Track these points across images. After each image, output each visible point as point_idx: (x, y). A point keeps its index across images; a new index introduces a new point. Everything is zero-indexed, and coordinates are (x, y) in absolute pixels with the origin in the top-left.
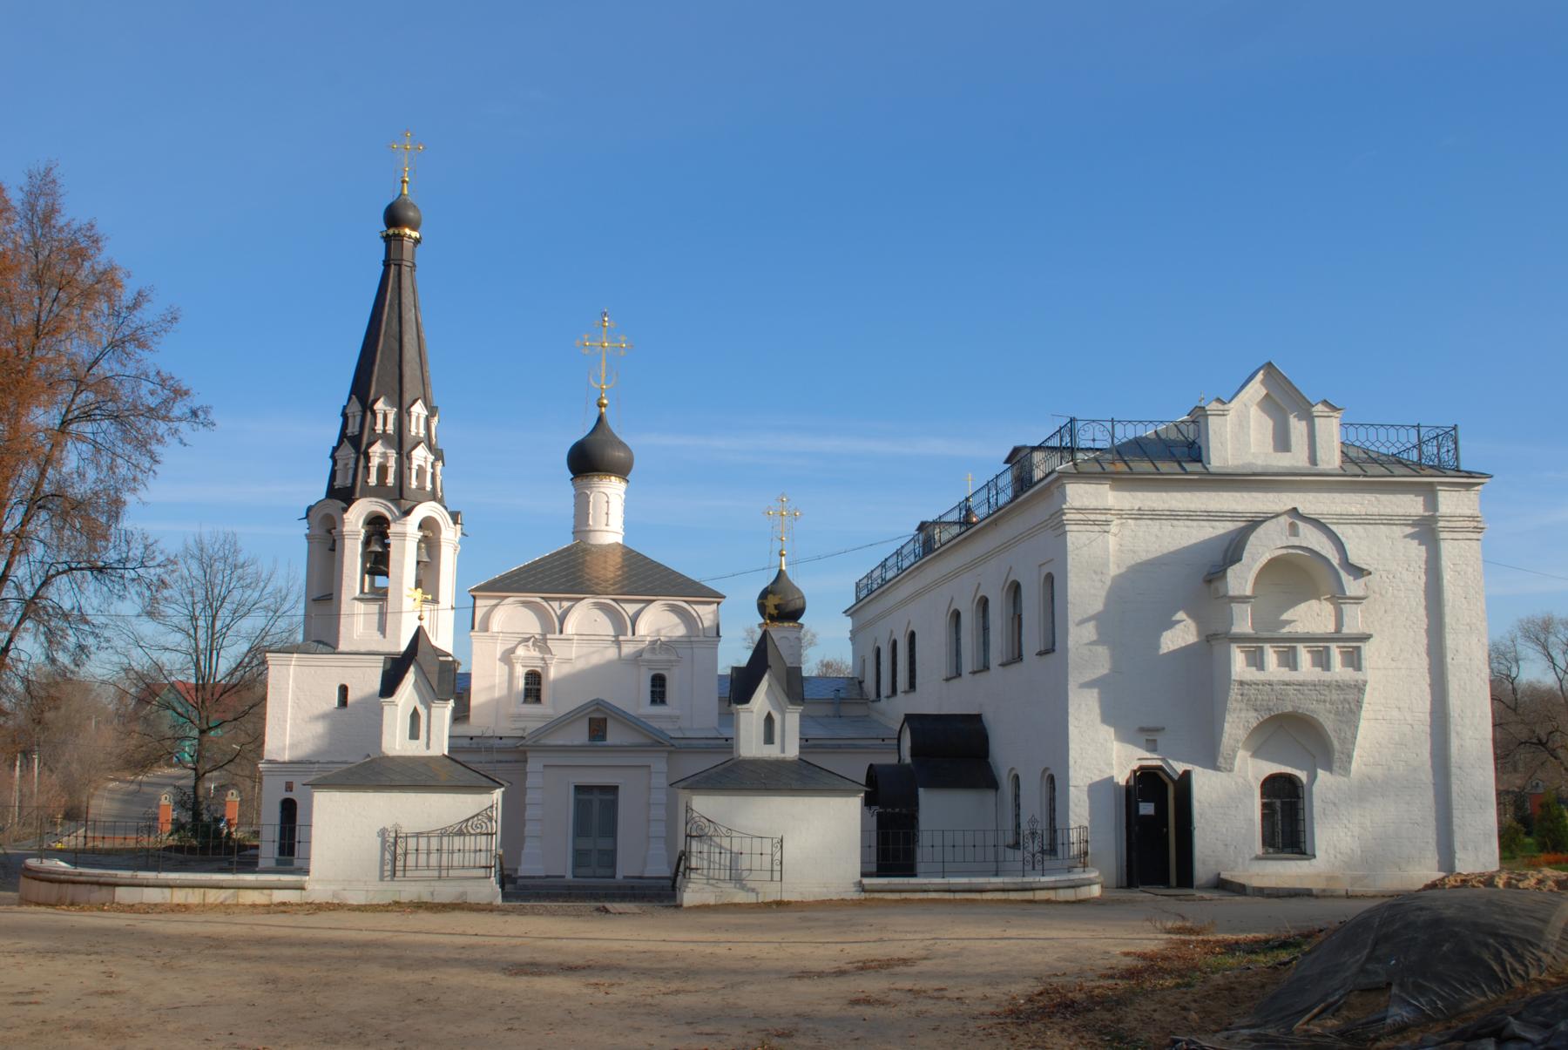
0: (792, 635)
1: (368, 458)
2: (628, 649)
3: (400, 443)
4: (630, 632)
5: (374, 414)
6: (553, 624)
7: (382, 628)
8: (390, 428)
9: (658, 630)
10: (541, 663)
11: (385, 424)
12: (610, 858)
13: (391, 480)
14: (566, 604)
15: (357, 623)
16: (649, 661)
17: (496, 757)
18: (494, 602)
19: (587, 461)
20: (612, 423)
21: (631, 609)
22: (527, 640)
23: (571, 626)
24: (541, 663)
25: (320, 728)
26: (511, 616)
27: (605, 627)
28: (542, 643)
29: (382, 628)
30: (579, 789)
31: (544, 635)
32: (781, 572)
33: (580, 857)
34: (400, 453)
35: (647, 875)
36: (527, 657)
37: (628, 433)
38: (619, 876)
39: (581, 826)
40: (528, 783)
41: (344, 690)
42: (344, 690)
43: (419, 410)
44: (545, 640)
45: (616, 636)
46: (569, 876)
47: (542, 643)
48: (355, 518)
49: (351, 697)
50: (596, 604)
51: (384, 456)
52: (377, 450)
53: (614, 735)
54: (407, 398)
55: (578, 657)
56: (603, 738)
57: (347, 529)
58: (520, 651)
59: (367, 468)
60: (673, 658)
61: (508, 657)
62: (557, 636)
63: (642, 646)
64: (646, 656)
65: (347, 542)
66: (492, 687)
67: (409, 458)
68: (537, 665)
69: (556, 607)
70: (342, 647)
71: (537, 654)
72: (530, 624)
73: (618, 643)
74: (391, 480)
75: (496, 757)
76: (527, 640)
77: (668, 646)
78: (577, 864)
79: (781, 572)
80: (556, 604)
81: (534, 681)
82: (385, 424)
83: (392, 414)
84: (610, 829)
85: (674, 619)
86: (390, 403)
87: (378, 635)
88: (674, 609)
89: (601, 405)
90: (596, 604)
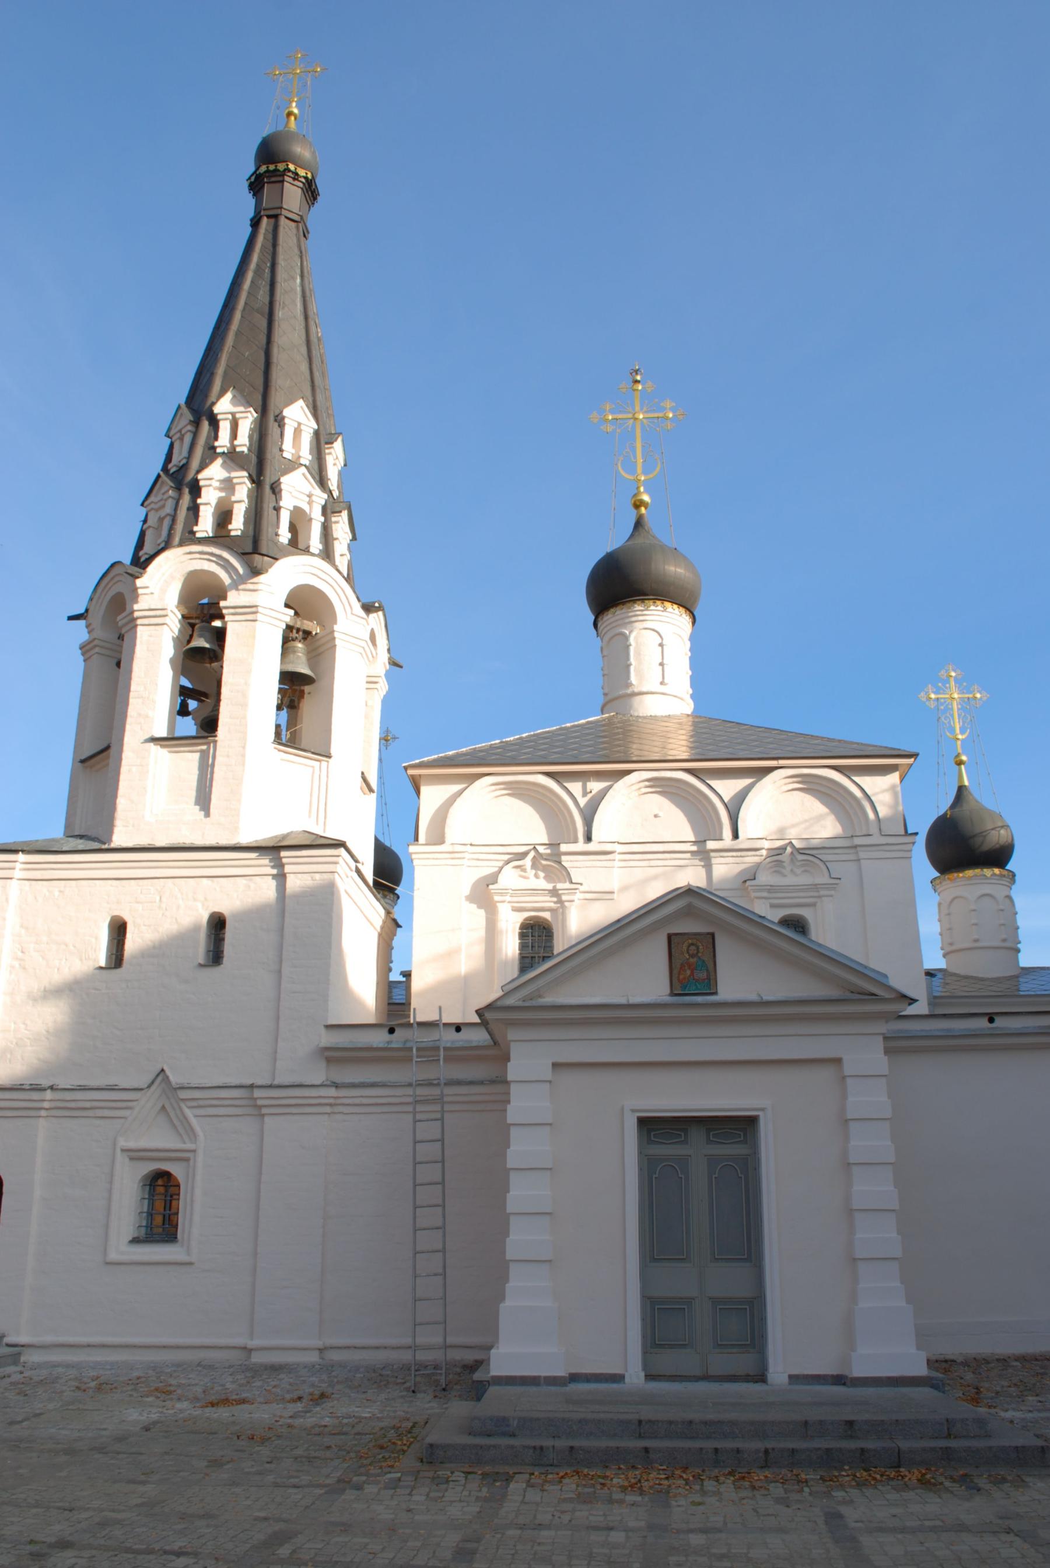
0: (999, 891)
1: (196, 490)
2: (724, 869)
3: (260, 464)
4: (727, 833)
5: (214, 422)
6: (568, 832)
7: (204, 799)
8: (243, 441)
9: (782, 831)
10: (549, 902)
11: (234, 435)
12: (746, 1320)
13: (237, 525)
14: (595, 786)
15: (153, 786)
16: (771, 889)
17: (444, 1071)
18: (456, 788)
19: (617, 586)
20: (659, 529)
21: (728, 788)
22: (523, 855)
23: (608, 824)
24: (549, 902)
25: (53, 1015)
26: (484, 820)
27: (676, 825)
28: (550, 861)
29: (204, 799)
30: (650, 1126)
31: (553, 845)
32: (961, 789)
33: (663, 1320)
34: (257, 480)
35: (858, 1370)
36: (522, 892)
37: (683, 546)
38: (778, 1372)
39: (662, 1236)
40: (514, 1112)
41: (119, 930)
42: (119, 930)
43: (297, 415)
44: (556, 856)
45: (700, 842)
46: (635, 1376)
47: (550, 861)
48: (162, 585)
49: (132, 943)
50: (654, 782)
51: (228, 485)
52: (215, 473)
53: (738, 978)
54: (276, 398)
55: (624, 889)
56: (710, 985)
57: (140, 606)
58: (510, 878)
59: (194, 510)
60: (823, 879)
61: (483, 894)
62: (581, 846)
63: (751, 859)
64: (764, 878)
65: (143, 634)
66: (451, 954)
67: (276, 489)
68: (542, 906)
69: (576, 793)
70: (119, 839)
71: (543, 884)
72: (528, 827)
73: (704, 856)
74: (237, 525)
75: (444, 1071)
76: (523, 855)
77: (809, 855)
78: (654, 1342)
79: (961, 789)
80: (575, 787)
81: (537, 935)
82: (234, 435)
83: (247, 421)
84: (744, 1242)
85: (815, 806)
86: (244, 398)
87: (197, 813)
88: (812, 786)
89: (638, 505)
90: (654, 782)
